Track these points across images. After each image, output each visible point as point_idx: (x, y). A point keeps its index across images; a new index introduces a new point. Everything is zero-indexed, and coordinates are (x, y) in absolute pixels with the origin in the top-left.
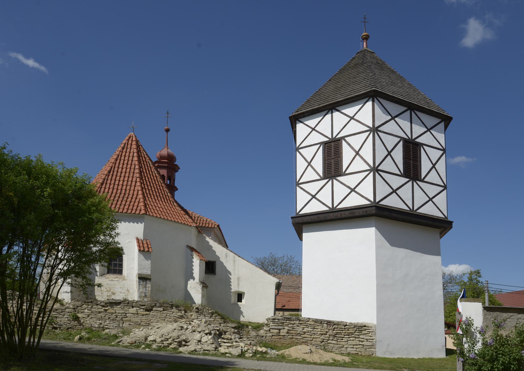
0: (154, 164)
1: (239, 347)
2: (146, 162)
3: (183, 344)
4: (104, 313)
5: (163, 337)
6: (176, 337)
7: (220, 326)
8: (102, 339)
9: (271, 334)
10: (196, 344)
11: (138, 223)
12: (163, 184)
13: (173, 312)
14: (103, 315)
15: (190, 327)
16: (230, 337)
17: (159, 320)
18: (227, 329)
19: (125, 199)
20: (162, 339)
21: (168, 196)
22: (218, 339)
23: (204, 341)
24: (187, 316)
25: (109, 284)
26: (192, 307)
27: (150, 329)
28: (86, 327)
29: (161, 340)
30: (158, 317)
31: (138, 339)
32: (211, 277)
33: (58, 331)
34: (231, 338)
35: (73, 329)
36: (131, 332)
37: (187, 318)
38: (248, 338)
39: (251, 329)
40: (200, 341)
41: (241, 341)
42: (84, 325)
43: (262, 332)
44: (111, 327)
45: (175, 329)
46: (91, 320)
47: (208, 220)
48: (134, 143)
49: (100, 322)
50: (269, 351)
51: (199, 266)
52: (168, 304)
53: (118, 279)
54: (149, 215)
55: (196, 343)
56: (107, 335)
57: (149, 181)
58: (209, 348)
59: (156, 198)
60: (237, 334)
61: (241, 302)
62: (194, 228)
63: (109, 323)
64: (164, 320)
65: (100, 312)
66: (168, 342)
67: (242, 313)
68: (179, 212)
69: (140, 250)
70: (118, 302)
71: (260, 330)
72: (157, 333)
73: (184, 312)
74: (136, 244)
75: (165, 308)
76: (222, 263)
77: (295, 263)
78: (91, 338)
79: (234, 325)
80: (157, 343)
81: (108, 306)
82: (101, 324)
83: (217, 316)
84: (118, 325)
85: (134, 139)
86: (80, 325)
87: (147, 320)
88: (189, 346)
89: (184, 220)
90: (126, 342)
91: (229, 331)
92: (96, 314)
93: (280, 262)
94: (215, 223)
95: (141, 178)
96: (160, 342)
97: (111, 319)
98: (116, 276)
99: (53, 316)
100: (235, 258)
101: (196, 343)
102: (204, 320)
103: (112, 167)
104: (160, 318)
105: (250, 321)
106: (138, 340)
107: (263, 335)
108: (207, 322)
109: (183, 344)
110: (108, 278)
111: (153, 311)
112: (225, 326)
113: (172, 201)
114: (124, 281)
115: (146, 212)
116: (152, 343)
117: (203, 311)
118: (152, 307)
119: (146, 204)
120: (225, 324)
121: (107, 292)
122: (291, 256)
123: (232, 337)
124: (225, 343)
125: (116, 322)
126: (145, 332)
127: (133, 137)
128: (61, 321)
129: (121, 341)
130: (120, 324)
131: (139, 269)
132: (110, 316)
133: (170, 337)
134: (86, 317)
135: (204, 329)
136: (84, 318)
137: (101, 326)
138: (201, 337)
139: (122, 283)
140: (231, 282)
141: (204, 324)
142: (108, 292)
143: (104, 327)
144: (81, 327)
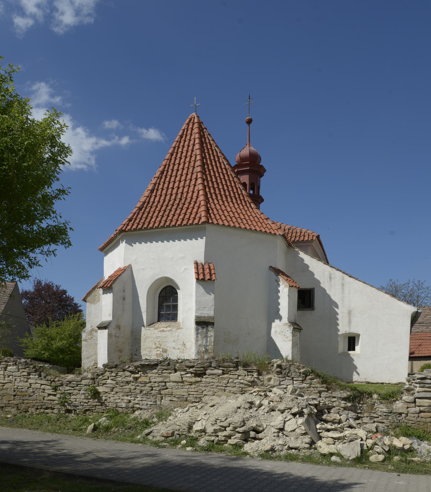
0: (233, 168)
1: (357, 439)
2: (212, 150)
3: (251, 436)
4: (133, 384)
5: (216, 423)
6: (239, 423)
7: (320, 397)
8: (126, 429)
9: (417, 409)
10: (274, 436)
11: (197, 239)
12: (235, 179)
13: (239, 376)
14: (133, 387)
15: (265, 402)
16: (338, 417)
17: (216, 390)
18: (333, 402)
19: (181, 206)
20: (216, 427)
21: (242, 194)
22: (316, 423)
23: (290, 430)
24: (261, 381)
25: (159, 337)
26: (270, 365)
27: (200, 409)
28: (109, 408)
29: (214, 430)
30: (214, 387)
31: (178, 427)
32: (307, 313)
33: (72, 416)
34: (340, 419)
35: (93, 411)
36: (170, 415)
37: (262, 385)
38: (372, 418)
39: (378, 399)
40: (282, 430)
41: (359, 424)
42: (107, 405)
43: (399, 406)
44: (143, 407)
45: (239, 408)
46: (116, 397)
47: (304, 230)
48: (196, 125)
49: (129, 398)
50: (416, 446)
51: (287, 298)
52: (231, 361)
53: (171, 329)
54: (213, 223)
55: (275, 434)
56: (135, 420)
57: (215, 175)
58: (298, 444)
59: (224, 199)
60: (352, 411)
61: (354, 350)
62: (280, 238)
63: (141, 400)
64: (225, 390)
65: (128, 383)
66: (225, 433)
67: (355, 368)
68: (259, 217)
69: (198, 279)
70: (153, 364)
71: (395, 401)
72: (208, 416)
73: (256, 374)
74: (193, 271)
75: (225, 369)
76: (324, 290)
77: (425, 290)
78: (111, 427)
79: (345, 395)
80: (207, 434)
81: (139, 371)
82: (130, 401)
83: (314, 379)
84: (154, 402)
85: (196, 120)
86: (101, 405)
87: (198, 392)
88: (263, 440)
89: (265, 226)
90: (159, 434)
91: (337, 406)
92: (122, 386)
93: (403, 291)
94: (313, 234)
95: (203, 172)
96: (212, 433)
97: (144, 392)
98: (168, 323)
99: (66, 392)
100: (343, 279)
101: (275, 434)
102: (290, 388)
103: (165, 166)
104: (218, 387)
105: (368, 380)
106: (176, 430)
107: (401, 411)
108: (296, 390)
109: (251, 436)
110: (157, 329)
111: (207, 376)
112: (329, 397)
113: (248, 201)
114: (179, 330)
115: (208, 219)
116: (199, 436)
117: (290, 371)
118: (205, 369)
119: (209, 208)
120: (330, 392)
121: (156, 350)
122: (419, 281)
123: (341, 417)
124: (328, 430)
125: (151, 397)
126: (190, 414)
127: (194, 118)
128: (76, 399)
129: (151, 432)
130: (157, 400)
131: (197, 310)
132: (142, 388)
133: (230, 424)
134: (110, 391)
135: (290, 405)
136: (107, 392)
137: (131, 405)
138: (285, 421)
139: (177, 334)
140: (338, 319)
141: (290, 395)
142: (158, 349)
143: (133, 407)
144: (104, 408)
